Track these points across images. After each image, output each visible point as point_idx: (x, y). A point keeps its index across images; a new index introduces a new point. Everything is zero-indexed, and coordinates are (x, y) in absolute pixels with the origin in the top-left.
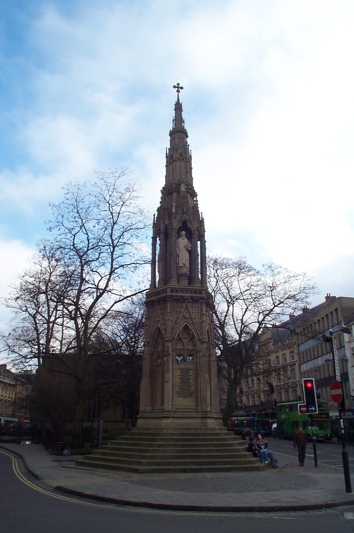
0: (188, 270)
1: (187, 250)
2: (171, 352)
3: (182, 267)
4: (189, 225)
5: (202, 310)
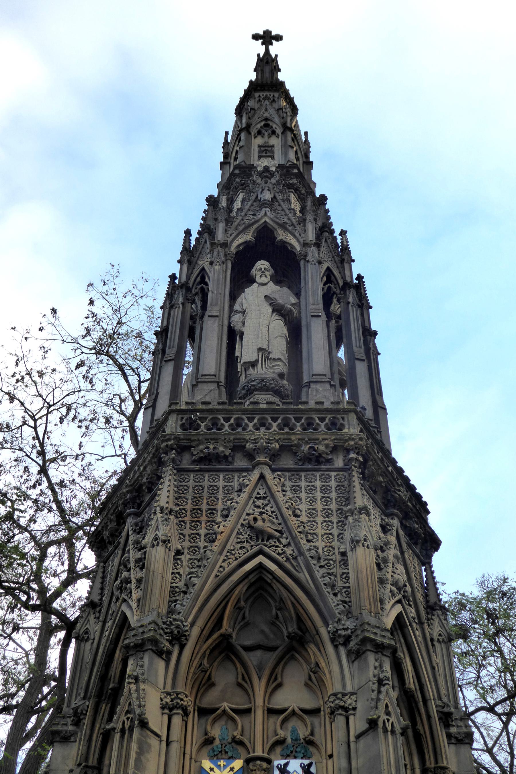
0: (281, 368)
1: (278, 310)
2: (156, 720)
5: (346, 498)
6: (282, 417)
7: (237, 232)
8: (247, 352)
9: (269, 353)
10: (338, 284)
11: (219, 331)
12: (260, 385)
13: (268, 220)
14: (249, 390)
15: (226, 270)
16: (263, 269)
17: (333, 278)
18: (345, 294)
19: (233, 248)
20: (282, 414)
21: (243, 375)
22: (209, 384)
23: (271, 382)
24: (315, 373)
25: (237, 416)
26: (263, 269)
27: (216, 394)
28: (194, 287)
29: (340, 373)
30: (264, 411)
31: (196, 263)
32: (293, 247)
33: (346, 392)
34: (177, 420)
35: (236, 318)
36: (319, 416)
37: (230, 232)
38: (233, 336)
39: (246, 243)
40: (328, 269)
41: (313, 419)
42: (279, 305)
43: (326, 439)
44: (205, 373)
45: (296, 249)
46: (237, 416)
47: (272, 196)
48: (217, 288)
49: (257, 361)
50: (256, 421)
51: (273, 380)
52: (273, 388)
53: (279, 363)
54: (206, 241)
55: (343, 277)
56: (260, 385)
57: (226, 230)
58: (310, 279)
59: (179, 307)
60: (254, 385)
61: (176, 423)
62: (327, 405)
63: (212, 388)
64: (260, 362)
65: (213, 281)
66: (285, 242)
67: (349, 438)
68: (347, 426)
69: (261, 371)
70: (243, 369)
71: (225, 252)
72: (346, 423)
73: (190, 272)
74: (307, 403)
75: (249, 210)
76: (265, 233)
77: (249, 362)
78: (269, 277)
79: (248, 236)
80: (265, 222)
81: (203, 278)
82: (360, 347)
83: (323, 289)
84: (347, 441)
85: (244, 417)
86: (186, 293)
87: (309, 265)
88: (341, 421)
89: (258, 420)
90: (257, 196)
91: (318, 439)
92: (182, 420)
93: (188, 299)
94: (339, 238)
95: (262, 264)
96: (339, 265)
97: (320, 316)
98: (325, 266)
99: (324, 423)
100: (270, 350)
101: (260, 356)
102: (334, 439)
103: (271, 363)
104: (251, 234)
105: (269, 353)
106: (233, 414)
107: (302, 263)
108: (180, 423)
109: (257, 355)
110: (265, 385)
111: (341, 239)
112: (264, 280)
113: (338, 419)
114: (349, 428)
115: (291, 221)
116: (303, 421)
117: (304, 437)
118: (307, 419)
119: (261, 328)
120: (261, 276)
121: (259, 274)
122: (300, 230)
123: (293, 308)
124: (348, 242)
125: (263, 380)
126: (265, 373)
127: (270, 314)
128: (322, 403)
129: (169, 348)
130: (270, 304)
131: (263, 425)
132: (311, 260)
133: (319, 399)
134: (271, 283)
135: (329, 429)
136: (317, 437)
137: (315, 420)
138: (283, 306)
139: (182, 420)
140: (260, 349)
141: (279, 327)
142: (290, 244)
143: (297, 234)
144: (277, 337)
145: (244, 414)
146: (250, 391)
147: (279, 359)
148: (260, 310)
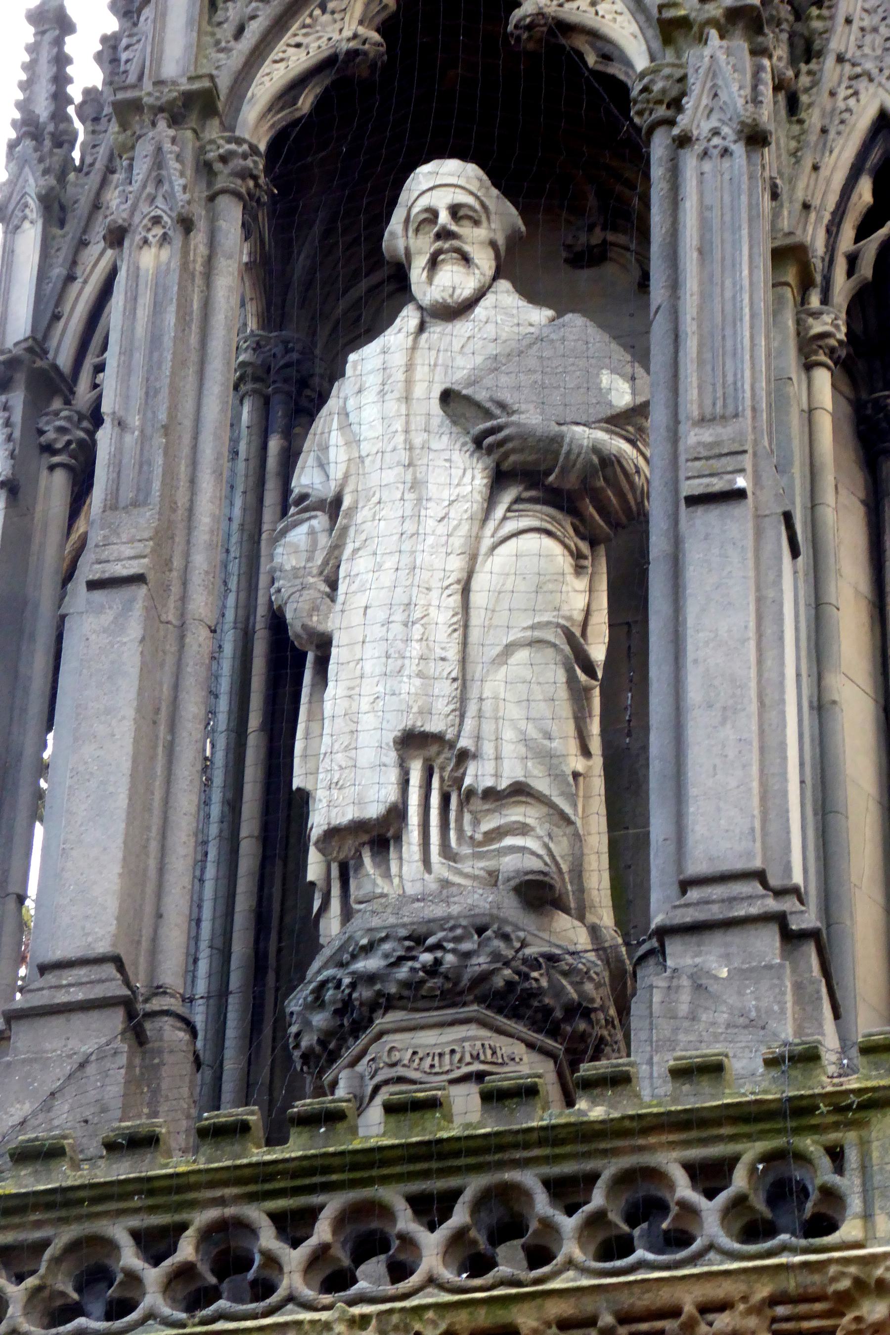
1: (526, 471)
6: (474, 1185)
8: (346, 767)
9: (464, 756)
11: (146, 671)
12: (403, 973)
14: (345, 1007)
15: (210, 261)
16: (444, 217)
19: (254, 120)
22: (78, 1020)
24: (696, 867)
26: (444, 217)
27: (110, 1084)
30: (371, 1164)
32: (609, 51)
35: (296, 548)
36: (695, 1153)
39: (336, 72)
41: (655, 1175)
42: (525, 439)
43: (723, 1306)
45: (628, 63)
48: (150, 393)
49: (396, 814)
50: (322, 1231)
51: (481, 930)
52: (484, 977)
53: (515, 814)
56: (403, 973)
60: (371, 978)
62: (749, 1081)
65: (127, 352)
66: (565, 28)
67: (859, 1284)
68: (855, 1204)
69: (411, 881)
71: (202, 150)
72: (850, 1184)
73: (58, 271)
74: (620, 1080)
77: (358, 827)
84: (844, 1301)
85: (256, 1214)
88: (825, 1174)
89: (340, 1223)
91: (674, 1312)
95: (442, 183)
97: (740, 494)
99: (723, 1197)
100: (464, 742)
102: (774, 1301)
103: (476, 822)
105: (464, 756)
106: (193, 1205)
107: (659, 147)
109: (393, 775)
110: (433, 970)
112: (452, 281)
113: (802, 1158)
114: (867, 1216)
116: (598, 1199)
117: (588, 1305)
118: (625, 1179)
120: (434, 263)
121: (422, 247)
123: (619, 445)
125: (418, 940)
126: (445, 883)
128: (713, 1069)
131: (368, 1245)
132: (702, 127)
133: (694, 1048)
134: (504, 295)
135: (754, 1230)
136: (665, 1297)
138: (551, 446)
140: (411, 741)
142: (594, 35)
144: (509, 649)
145: (253, 1198)
146: (354, 1019)
147: (520, 791)
148: (416, 485)
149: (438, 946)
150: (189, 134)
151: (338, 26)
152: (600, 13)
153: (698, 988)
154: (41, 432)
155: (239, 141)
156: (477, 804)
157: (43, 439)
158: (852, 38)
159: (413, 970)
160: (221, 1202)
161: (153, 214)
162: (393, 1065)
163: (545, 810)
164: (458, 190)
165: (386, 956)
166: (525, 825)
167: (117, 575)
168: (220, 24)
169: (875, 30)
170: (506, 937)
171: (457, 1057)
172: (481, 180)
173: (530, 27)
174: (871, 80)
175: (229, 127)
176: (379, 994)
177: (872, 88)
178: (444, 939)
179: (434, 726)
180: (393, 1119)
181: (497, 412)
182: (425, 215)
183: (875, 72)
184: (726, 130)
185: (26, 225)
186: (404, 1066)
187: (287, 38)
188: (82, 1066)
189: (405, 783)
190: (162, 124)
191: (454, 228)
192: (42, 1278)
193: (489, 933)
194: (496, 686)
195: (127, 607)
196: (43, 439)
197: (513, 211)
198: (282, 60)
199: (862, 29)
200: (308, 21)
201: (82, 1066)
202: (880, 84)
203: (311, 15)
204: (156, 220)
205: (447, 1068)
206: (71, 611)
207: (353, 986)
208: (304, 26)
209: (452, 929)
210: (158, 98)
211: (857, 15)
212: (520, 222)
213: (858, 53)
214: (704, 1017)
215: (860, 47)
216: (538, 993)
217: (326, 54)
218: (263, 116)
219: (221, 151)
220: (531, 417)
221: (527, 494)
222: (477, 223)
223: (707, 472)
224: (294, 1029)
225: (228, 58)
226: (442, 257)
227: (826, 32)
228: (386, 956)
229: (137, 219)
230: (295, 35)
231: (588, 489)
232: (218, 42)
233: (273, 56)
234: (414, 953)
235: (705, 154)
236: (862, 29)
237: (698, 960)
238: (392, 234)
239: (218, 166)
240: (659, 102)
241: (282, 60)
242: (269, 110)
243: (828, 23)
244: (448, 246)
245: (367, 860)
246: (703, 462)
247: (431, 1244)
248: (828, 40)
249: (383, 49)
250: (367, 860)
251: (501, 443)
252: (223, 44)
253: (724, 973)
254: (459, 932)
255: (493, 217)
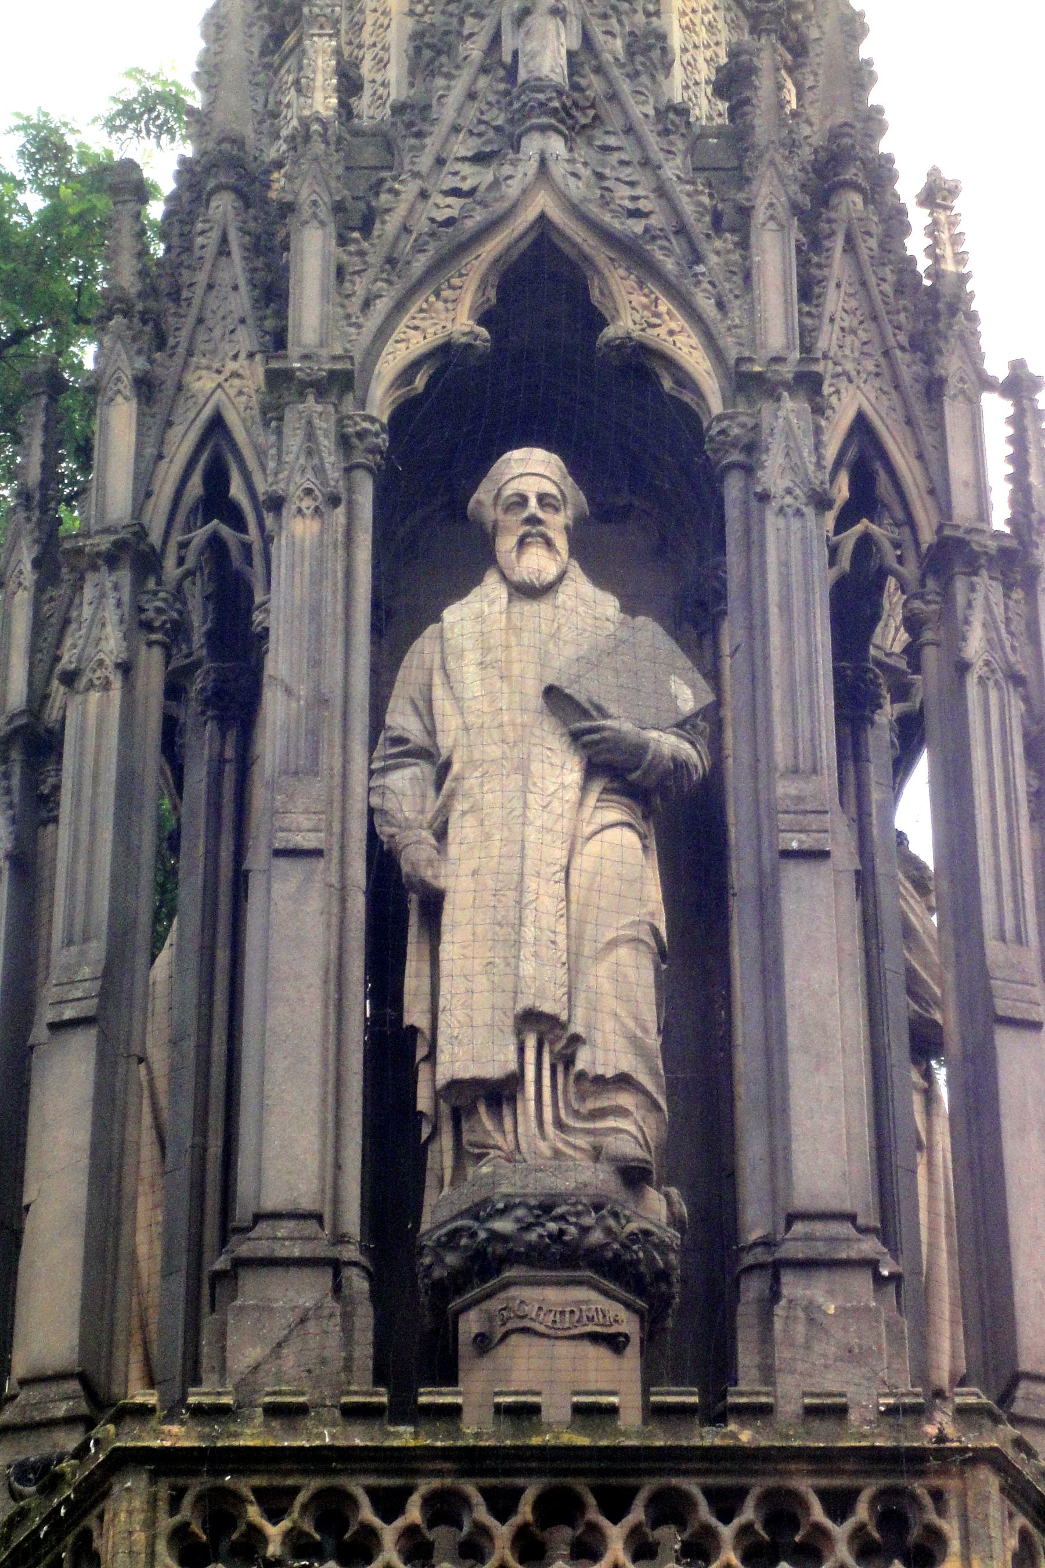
1: (613, 767)
3: (500, 1094)
4: (634, 312)
7: (399, 287)
9: (576, 1040)
10: (910, 522)
13: (557, 215)
17: (883, 485)
18: (947, 595)
19: (380, 400)
20: (651, 1473)
21: (446, 1140)
23: (588, 1220)
25: (436, 1483)
28: (176, 538)
29: (913, 986)
31: (180, 388)
32: (684, 379)
33: (941, 1075)
34: (153, 1502)
36: (824, 1482)
37: (360, 286)
38: (397, 909)
39: (445, 353)
40: (861, 425)
41: (797, 1499)
42: (617, 742)
44: (271, 1202)
46: (436, 1483)
47: (576, 44)
51: (598, 1207)
53: (625, 1099)
54: (224, 240)
55: (939, 492)
56: (533, 1236)
57: (340, 272)
58: (774, 611)
59: (106, 686)
61: (150, 1524)
63: (307, 1300)
64: (530, 1089)
68: (955, 1545)
70: (445, 1108)
72: (951, 1528)
73: (150, 451)
75: (456, 129)
76: (544, 285)
77: (476, 1083)
78: (561, 543)
79: (453, 316)
80: (542, 217)
81: (217, 479)
82: (1020, 938)
83: (834, 551)
85: (470, 1488)
86: (138, 583)
87: (770, 518)
90: (496, 40)
92: (174, 1505)
93: (147, 626)
94: (918, 218)
95: (531, 470)
96: (918, 409)
98: (846, 405)
100: (577, 1028)
101: (530, 1055)
103: (582, 1098)
104: (468, 299)
106: (416, 1473)
108: (166, 1523)
109: (512, 1049)
111: (933, 230)
113: (914, 1498)
115: (675, 211)
119: (531, 884)
120: (522, 543)
122: (720, 276)
124: (960, 259)
125: (546, 1208)
127: (572, 795)
129: (69, 942)
130: (576, 736)
137: (806, 1507)
139: (174, 1505)
140: (530, 1020)
141: (621, 862)
143: (706, 305)
147: (624, 1081)
149: (562, 1218)
150: (331, 408)
151: (451, 315)
152: (678, 345)
153: (811, 1321)
154: (141, 610)
155: (373, 420)
156: (587, 1085)
157: (143, 617)
158: (834, 336)
159: (541, 1236)
160: (439, 1473)
161: (305, 486)
162: (524, 1317)
163: (641, 1097)
164: (544, 480)
165: (518, 1220)
166: (627, 1110)
167: (299, 846)
168: (348, 296)
169: (853, 332)
170: (615, 1215)
171: (576, 1317)
172: (560, 469)
173: (619, 348)
174: (850, 381)
175: (362, 404)
176: (510, 1251)
177: (852, 388)
178: (569, 1213)
179: (547, 1008)
180: (579, 1419)
181: (595, 713)
182: (515, 499)
183: (853, 374)
184: (798, 491)
185: (119, 399)
186: (532, 1319)
187: (406, 320)
188: (303, 1321)
189: (521, 1050)
190: (311, 399)
191: (541, 515)
192: (294, 1522)
193: (604, 1212)
194: (599, 976)
195: (308, 880)
196: (143, 617)
197: (584, 499)
198: (403, 341)
199: (843, 329)
200: (425, 306)
201: (303, 1321)
202: (858, 387)
203: (426, 301)
204: (309, 492)
205: (567, 1325)
206: (256, 867)
207: (488, 1240)
208: (421, 310)
209: (574, 1205)
210: (308, 375)
211: (839, 314)
212: (586, 506)
213: (840, 354)
214: (816, 1348)
215: (840, 347)
216: (635, 1263)
217: (441, 341)
218: (387, 391)
219: (358, 428)
220: (621, 723)
221: (610, 786)
222: (557, 510)
223: (796, 828)
224: (427, 1260)
225: (359, 334)
226: (529, 540)
227: (813, 330)
228: (518, 1220)
229: (292, 489)
230: (414, 318)
231: (661, 787)
232: (348, 316)
233: (394, 337)
234: (541, 1220)
235: (781, 510)
236: (843, 329)
237: (808, 1292)
238: (479, 502)
239: (355, 441)
240: (734, 445)
241: (403, 341)
242: (392, 386)
243: (817, 322)
244: (533, 532)
245: (482, 1109)
246: (792, 816)
247: (616, 1536)
248: (817, 338)
249: (488, 344)
250: (482, 1109)
251: (596, 743)
252: (354, 320)
253: (832, 1311)
254: (580, 1207)
255: (569, 506)
